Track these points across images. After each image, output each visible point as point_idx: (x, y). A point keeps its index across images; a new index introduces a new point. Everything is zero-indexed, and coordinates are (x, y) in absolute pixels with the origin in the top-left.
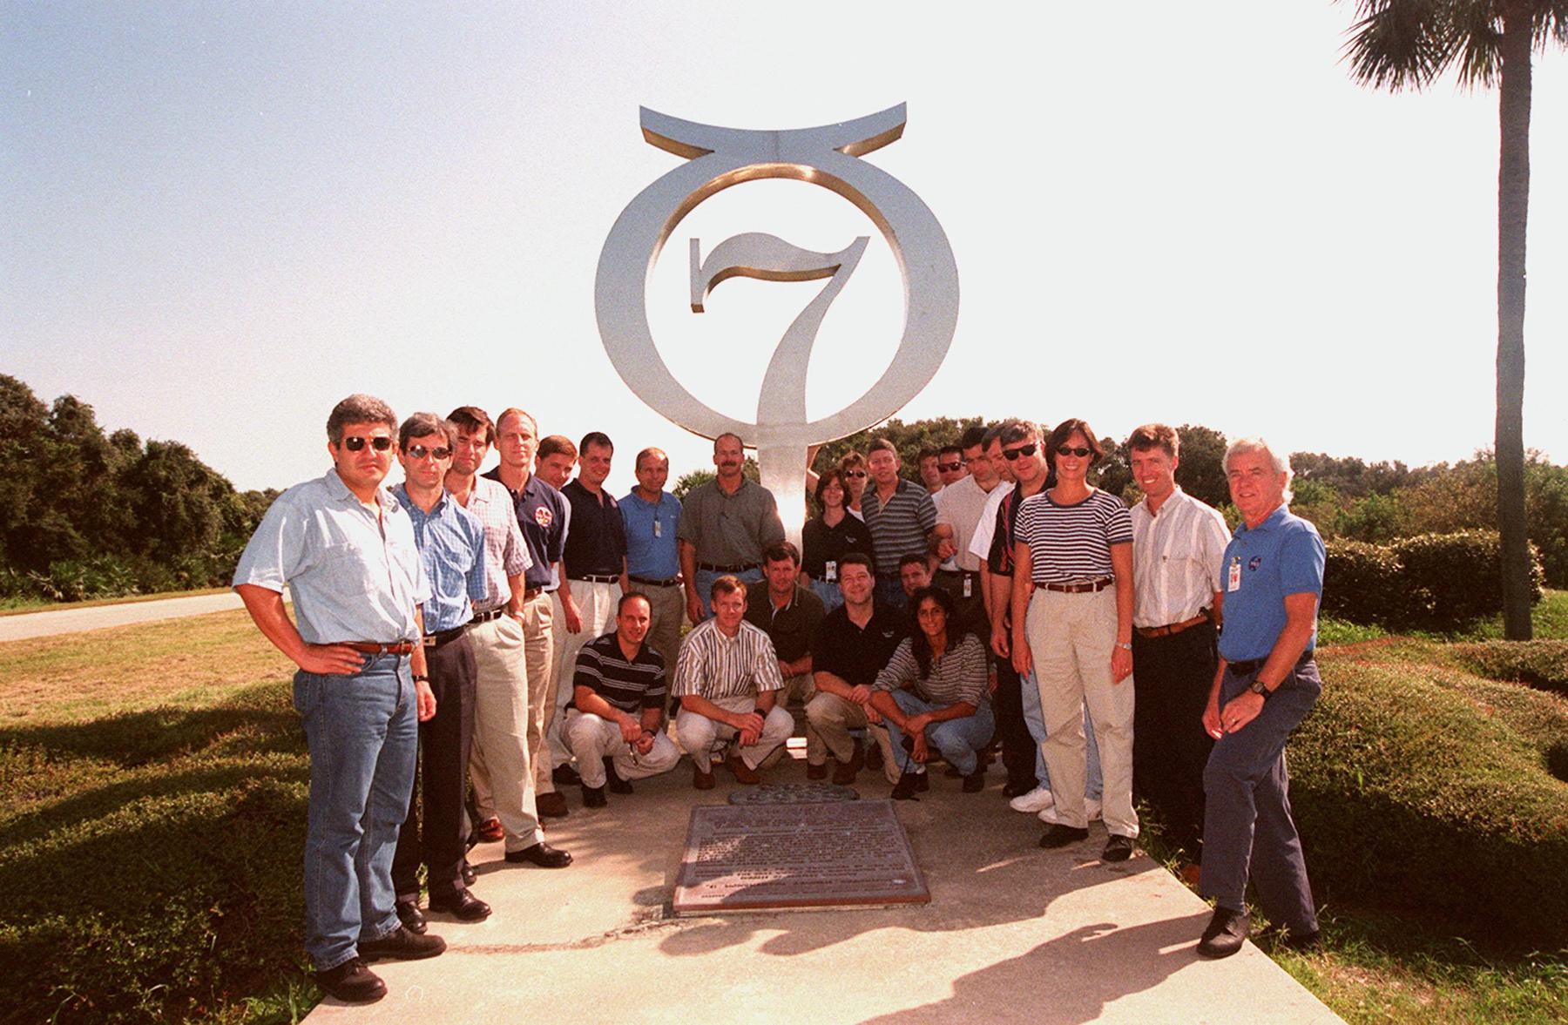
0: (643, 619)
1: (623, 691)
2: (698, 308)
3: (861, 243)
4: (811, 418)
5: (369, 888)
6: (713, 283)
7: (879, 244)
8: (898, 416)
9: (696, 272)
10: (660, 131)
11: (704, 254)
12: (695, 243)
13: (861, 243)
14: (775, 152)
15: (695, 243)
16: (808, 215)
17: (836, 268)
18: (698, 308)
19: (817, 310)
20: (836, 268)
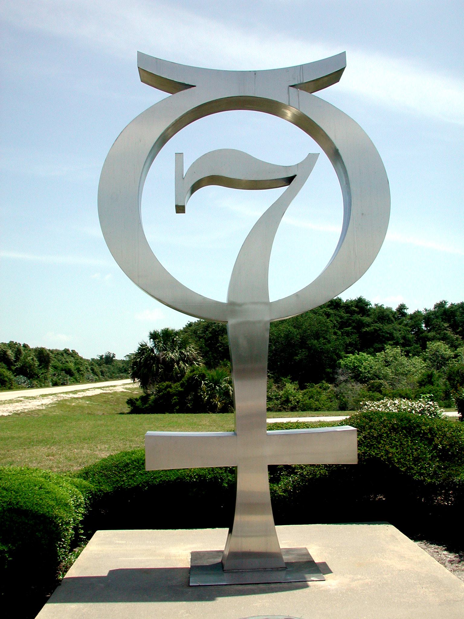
0: (64, 575)
1: (287, 423)
2: (180, 209)
3: (312, 159)
4: (272, 298)
5: (216, 324)
6: (195, 188)
7: (324, 161)
8: (339, 296)
9: (179, 177)
10: (159, 77)
11: (186, 168)
12: (179, 156)
13: (312, 159)
14: (248, 98)
15: (179, 156)
16: (272, 140)
17: (289, 180)
18: (180, 209)
19: (267, 226)
20: (289, 180)
